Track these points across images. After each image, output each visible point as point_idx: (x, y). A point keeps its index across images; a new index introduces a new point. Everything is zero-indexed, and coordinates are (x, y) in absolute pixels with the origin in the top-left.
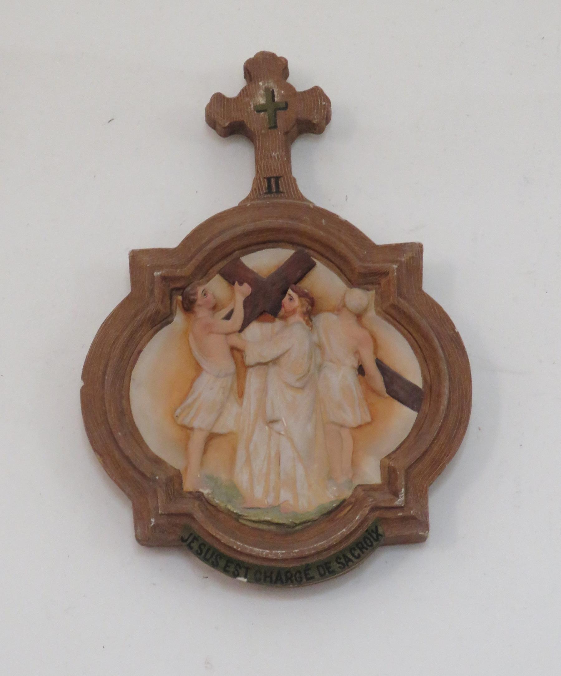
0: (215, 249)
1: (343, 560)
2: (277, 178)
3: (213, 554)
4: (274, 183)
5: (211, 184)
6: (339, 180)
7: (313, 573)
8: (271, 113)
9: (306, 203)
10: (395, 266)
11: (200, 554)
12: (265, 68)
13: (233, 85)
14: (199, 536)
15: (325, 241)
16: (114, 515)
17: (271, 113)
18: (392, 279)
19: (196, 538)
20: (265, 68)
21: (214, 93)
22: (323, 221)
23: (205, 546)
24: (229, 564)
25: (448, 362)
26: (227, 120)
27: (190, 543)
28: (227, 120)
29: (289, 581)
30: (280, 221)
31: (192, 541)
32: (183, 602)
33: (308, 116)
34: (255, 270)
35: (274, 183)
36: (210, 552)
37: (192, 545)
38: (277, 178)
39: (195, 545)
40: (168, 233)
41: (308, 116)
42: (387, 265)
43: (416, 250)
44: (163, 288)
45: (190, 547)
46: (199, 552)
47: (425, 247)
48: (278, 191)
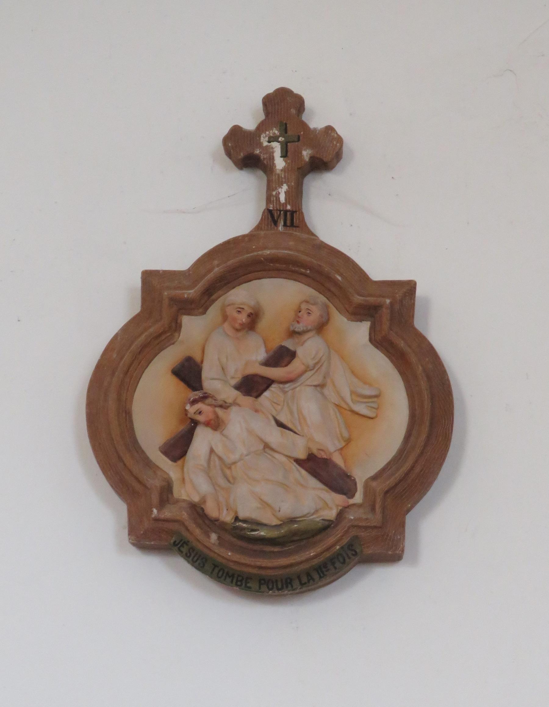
0: (230, 267)
3: (200, 556)
4: (285, 216)
5: (232, 208)
6: (335, 215)
7: (185, 549)
8: (285, 144)
10: (388, 301)
11: (189, 557)
12: (283, 107)
13: (249, 119)
14: (188, 542)
15: (332, 276)
17: (285, 144)
18: (391, 314)
19: (186, 543)
20: (283, 107)
21: (266, 94)
22: (352, 518)
23: (193, 550)
25: (130, 346)
26: (242, 150)
27: (180, 547)
28: (242, 150)
30: (388, 482)
31: (182, 546)
33: (321, 154)
35: (285, 216)
37: (182, 549)
40: (180, 252)
41: (321, 154)
42: (379, 300)
43: (409, 288)
44: (167, 302)
45: (180, 552)
46: (188, 555)
47: (419, 292)
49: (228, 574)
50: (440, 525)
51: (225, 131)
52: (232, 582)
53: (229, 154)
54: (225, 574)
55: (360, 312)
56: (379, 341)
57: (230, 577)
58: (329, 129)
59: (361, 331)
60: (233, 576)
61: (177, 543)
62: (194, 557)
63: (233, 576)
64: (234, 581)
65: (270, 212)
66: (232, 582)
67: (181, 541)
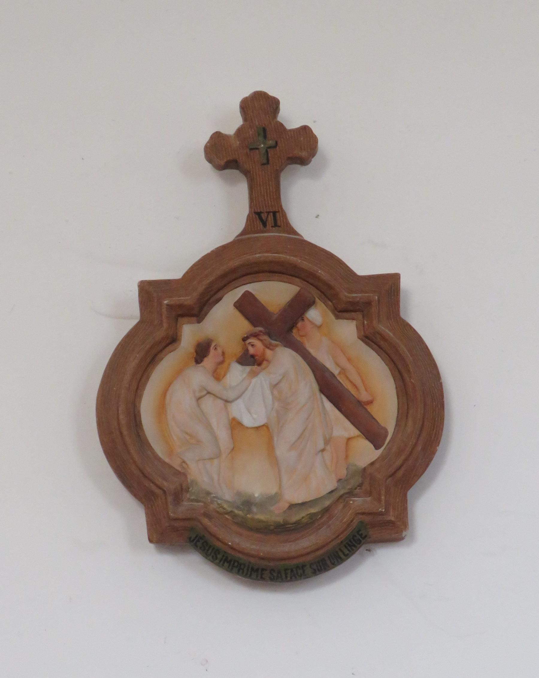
0: (215, 276)
1: (275, 575)
2: (274, 213)
3: (292, 570)
4: (267, 214)
5: (210, 215)
6: (327, 213)
7: (308, 570)
8: (263, 148)
9: (301, 238)
12: (260, 108)
13: (291, 117)
16: (425, 312)
17: (263, 148)
18: (374, 304)
20: (260, 108)
21: (265, 91)
23: (200, 548)
24: (263, 572)
26: (222, 154)
28: (222, 154)
29: (229, 558)
31: (198, 541)
32: (190, 587)
33: (301, 147)
34: (263, 302)
35: (267, 214)
36: (211, 549)
38: (274, 213)
39: (199, 544)
40: (172, 262)
44: (167, 312)
45: (196, 546)
47: (404, 283)
48: (276, 225)
49: (252, 569)
50: (433, 505)
51: (205, 139)
52: (257, 576)
53: (210, 160)
54: (250, 570)
55: (343, 310)
56: (370, 338)
57: (227, 562)
58: (305, 130)
59: (347, 330)
60: (229, 562)
61: (192, 539)
62: (208, 550)
63: (257, 570)
64: (259, 576)
65: (259, 214)
66: (243, 573)
67: (196, 537)
